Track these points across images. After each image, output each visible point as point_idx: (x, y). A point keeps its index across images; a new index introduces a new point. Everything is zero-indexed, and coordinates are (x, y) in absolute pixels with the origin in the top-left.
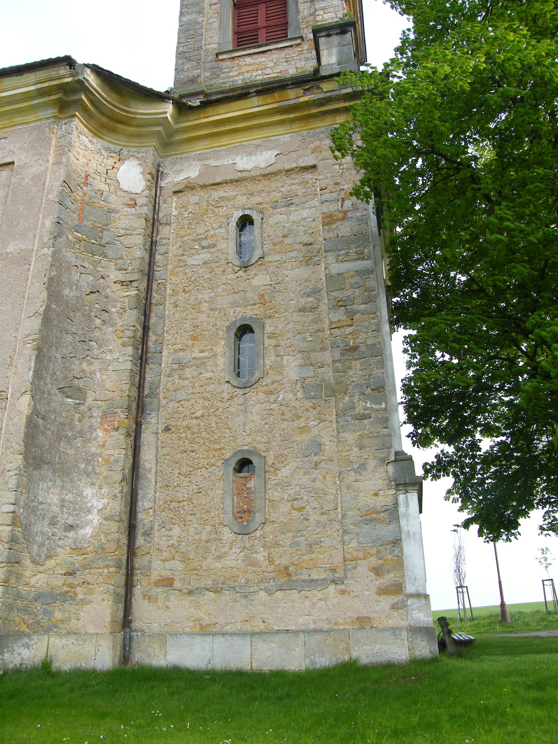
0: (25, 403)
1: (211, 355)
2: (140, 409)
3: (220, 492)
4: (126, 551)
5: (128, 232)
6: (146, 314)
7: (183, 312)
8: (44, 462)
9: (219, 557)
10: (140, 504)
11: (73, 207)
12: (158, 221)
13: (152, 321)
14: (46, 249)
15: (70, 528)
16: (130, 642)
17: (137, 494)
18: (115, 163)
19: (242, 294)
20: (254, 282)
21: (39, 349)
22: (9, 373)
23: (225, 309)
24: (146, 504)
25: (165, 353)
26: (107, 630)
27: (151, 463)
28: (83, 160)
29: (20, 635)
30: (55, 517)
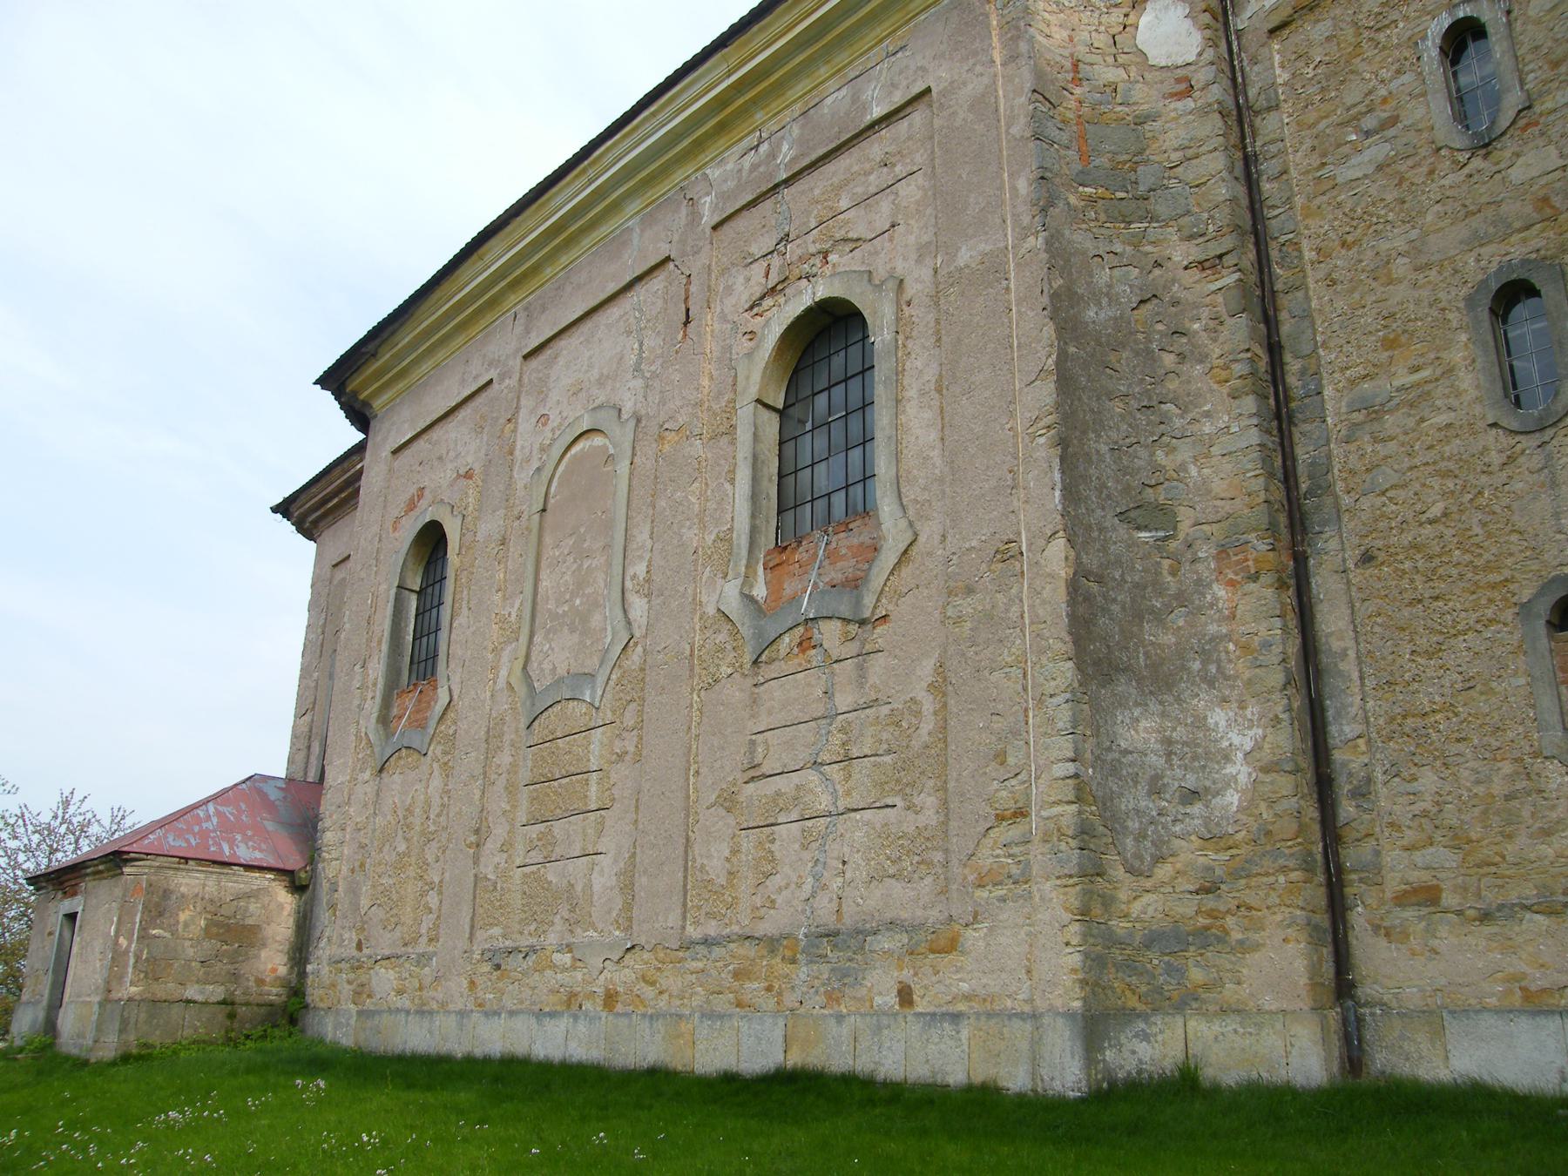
0: (1056, 557)
1: (1439, 372)
2: (1298, 528)
3: (1522, 681)
4: (1318, 835)
5: (1190, 153)
6: (1269, 320)
7: (1352, 291)
8: (1117, 670)
9: (1546, 833)
10: (1333, 729)
11: (1064, 137)
12: (1249, 108)
13: (1286, 328)
14: (1032, 239)
15: (1192, 796)
16: (1358, 1030)
17: (1323, 710)
18: (1126, 15)
19: (1489, 212)
20: (1517, 174)
21: (1063, 443)
22: (1015, 503)
23: (1452, 260)
24: (1347, 729)
25: (1328, 392)
26: (1305, 1004)
27: (1342, 639)
28: (1060, 35)
29: (1128, 1015)
30: (1156, 778)
